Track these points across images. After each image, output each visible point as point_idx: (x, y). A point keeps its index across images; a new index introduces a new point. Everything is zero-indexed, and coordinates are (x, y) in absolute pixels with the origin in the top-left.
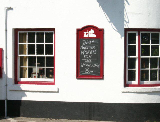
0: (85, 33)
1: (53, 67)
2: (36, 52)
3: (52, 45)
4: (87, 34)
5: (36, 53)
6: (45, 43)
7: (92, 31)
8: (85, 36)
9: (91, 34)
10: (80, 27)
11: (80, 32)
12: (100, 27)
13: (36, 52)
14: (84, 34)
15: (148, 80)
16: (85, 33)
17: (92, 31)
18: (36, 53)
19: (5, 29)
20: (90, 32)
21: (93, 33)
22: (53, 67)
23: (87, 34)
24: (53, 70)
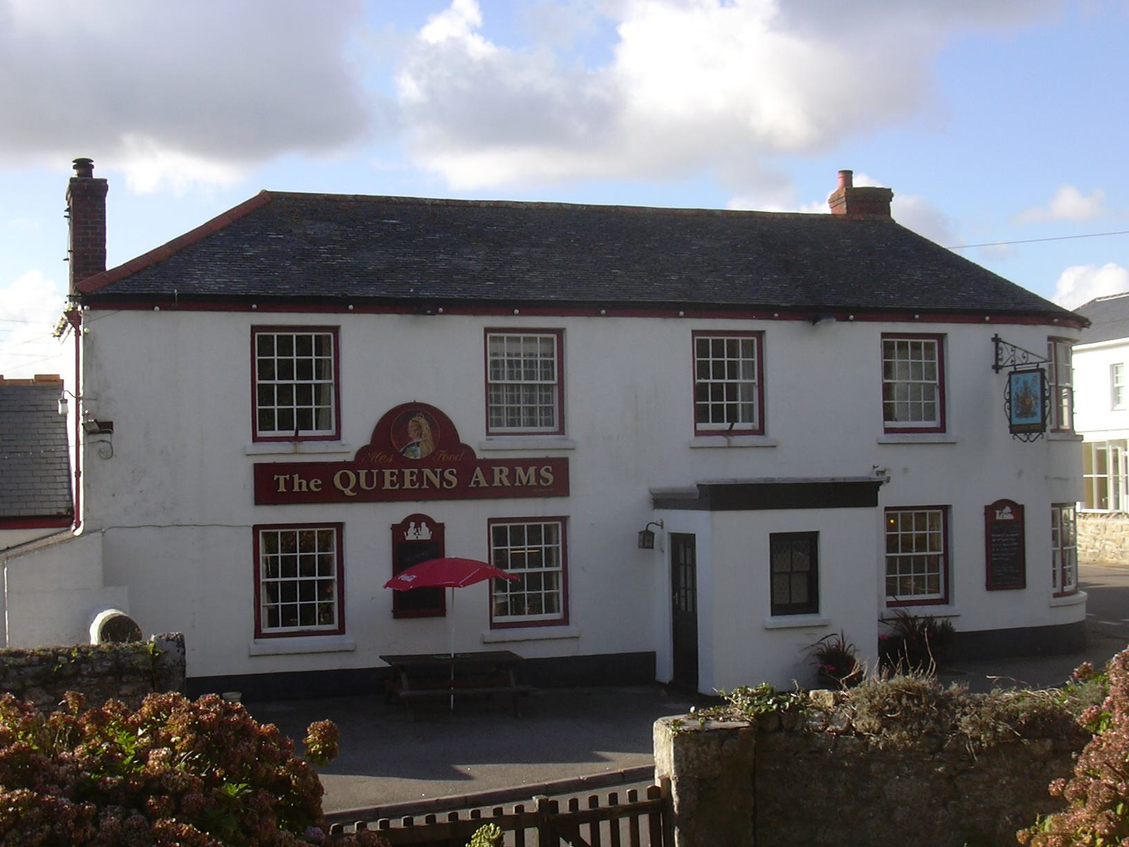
0: (998, 512)
1: (698, 403)
2: (303, 603)
3: (698, 357)
4: (1000, 514)
5: (928, 550)
6: (295, 407)
7: (1008, 509)
8: (998, 517)
9: (1006, 515)
10: (990, 503)
11: (990, 511)
12: (1019, 502)
13: (303, 603)
14: (996, 513)
15: (278, 626)
16: (998, 512)
17: (1008, 509)
18: (928, 550)
19: (10, 545)
20: (1005, 511)
21: (1009, 513)
22: (698, 403)
23: (1000, 514)
24: (697, 398)
